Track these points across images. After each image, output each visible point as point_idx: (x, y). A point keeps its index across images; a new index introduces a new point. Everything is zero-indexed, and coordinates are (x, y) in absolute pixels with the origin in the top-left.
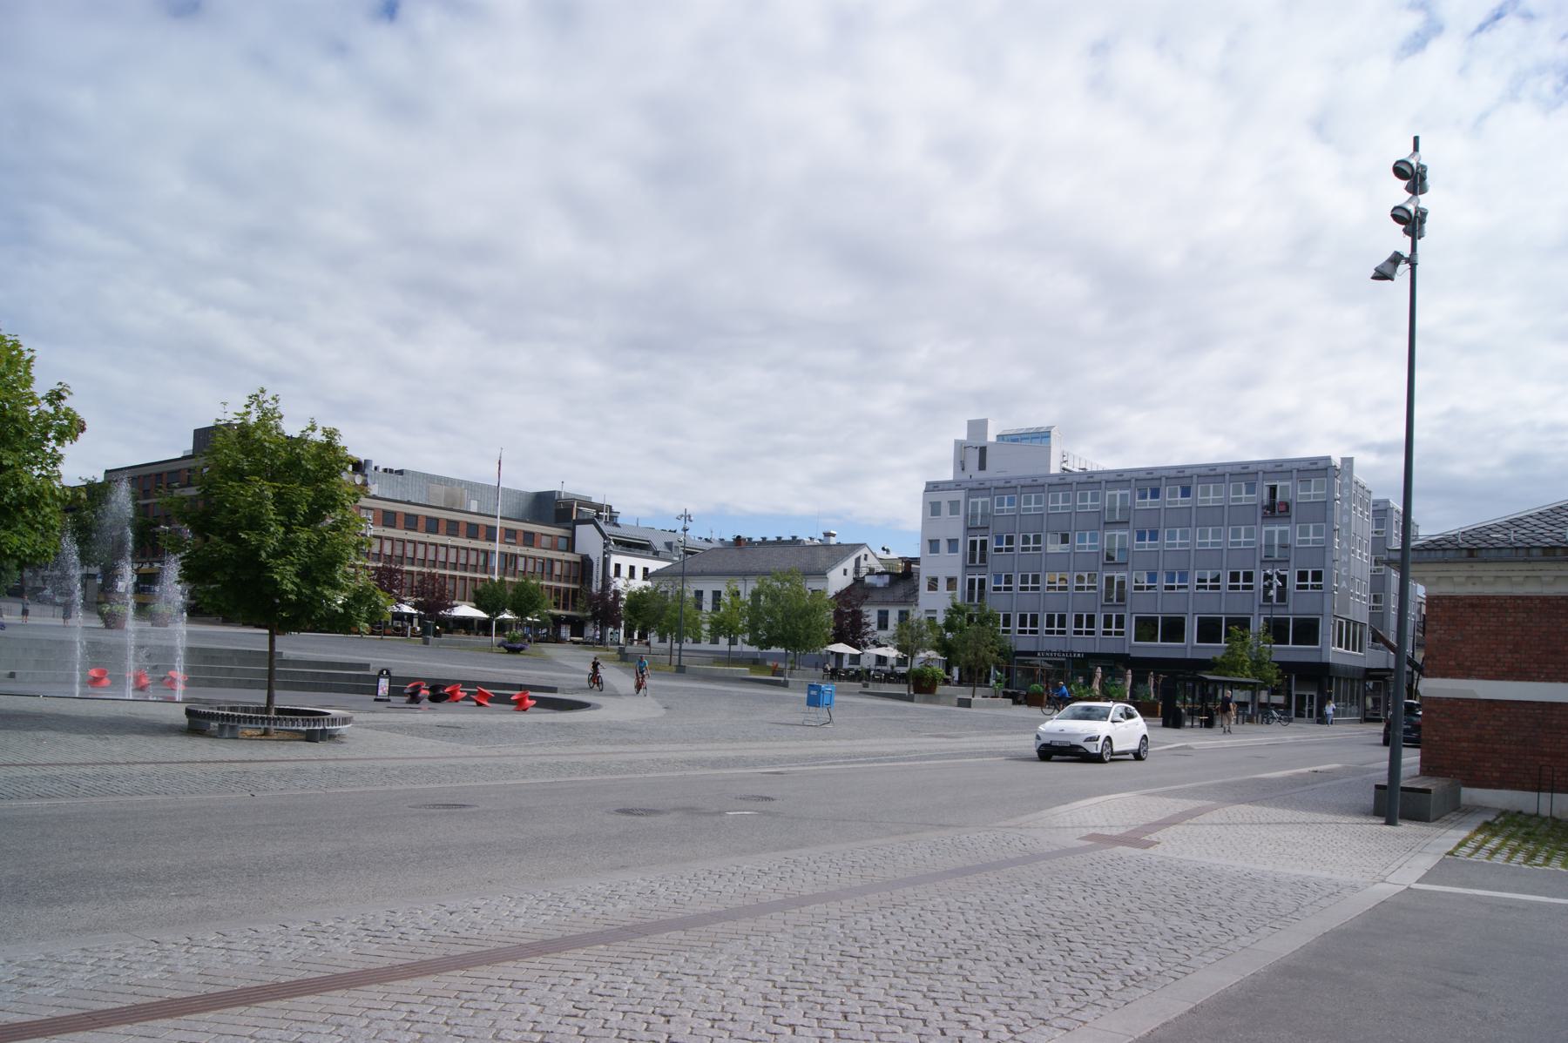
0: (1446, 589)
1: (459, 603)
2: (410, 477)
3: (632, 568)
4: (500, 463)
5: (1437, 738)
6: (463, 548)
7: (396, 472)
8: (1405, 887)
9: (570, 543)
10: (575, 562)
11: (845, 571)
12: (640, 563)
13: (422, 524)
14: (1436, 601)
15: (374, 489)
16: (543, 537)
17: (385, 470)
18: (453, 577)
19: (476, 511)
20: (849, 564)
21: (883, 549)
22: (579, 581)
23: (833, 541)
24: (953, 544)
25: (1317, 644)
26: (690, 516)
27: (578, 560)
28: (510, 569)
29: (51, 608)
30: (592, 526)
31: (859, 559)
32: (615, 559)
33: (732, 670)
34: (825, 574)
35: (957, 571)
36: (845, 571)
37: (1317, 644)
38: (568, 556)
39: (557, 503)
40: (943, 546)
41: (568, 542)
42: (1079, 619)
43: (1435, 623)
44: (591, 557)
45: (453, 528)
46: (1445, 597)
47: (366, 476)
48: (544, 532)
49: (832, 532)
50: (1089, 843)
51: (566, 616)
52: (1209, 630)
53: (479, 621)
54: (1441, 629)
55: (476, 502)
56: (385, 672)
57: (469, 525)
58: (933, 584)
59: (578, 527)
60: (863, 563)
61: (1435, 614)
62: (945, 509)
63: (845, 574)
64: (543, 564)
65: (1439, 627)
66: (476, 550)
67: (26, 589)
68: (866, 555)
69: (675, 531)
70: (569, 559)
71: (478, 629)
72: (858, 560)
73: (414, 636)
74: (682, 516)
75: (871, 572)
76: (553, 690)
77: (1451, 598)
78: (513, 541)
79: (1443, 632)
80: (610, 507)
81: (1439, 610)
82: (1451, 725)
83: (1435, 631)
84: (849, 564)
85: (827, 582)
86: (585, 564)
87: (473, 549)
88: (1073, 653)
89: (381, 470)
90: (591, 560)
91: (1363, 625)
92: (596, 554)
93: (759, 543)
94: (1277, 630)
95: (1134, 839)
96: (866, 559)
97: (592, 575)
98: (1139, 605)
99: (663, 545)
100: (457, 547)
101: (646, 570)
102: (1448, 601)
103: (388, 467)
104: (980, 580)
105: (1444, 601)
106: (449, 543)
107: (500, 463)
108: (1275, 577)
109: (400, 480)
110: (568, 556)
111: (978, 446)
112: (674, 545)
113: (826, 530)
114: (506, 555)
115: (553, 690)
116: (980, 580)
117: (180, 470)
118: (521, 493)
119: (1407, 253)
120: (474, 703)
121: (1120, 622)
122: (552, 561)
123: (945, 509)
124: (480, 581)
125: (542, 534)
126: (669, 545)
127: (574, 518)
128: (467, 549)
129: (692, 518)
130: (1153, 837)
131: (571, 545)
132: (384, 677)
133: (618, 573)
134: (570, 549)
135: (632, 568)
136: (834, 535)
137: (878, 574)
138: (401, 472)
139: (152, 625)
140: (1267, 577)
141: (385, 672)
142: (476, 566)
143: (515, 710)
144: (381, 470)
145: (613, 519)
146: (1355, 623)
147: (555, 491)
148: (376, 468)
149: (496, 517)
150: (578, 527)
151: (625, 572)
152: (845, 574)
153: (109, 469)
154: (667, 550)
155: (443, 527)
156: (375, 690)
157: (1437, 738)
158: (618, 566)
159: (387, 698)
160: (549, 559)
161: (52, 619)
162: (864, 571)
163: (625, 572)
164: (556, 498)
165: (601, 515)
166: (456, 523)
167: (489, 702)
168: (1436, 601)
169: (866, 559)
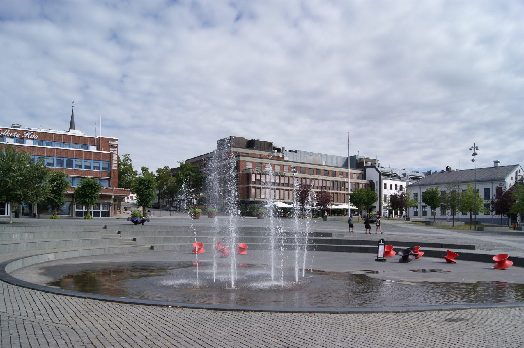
1: (343, 204)
2: (300, 153)
3: (391, 185)
4: (348, 139)
6: (324, 180)
7: (294, 151)
9: (364, 176)
10: (367, 184)
11: (512, 177)
12: (394, 183)
15: (286, 159)
16: (353, 174)
17: (290, 151)
18: (333, 193)
19: (325, 165)
20: (513, 174)
23: (499, 165)
25: (76, 216)
26: (477, 147)
27: (369, 183)
28: (343, 188)
29: (170, 212)
30: (373, 169)
32: (384, 182)
33: (502, 228)
34: (504, 179)
36: (512, 177)
37: (76, 216)
38: (364, 181)
39: (357, 160)
41: (363, 176)
44: (374, 181)
45: (319, 172)
47: (283, 153)
48: (353, 172)
49: (498, 161)
53: (332, 210)
55: (325, 162)
56: (382, 241)
59: (367, 170)
60: (518, 174)
63: (512, 179)
64: (355, 185)
66: (330, 181)
67: (161, 206)
68: (519, 170)
69: (405, 169)
70: (365, 183)
71: (331, 213)
72: (516, 173)
73: (314, 217)
74: (472, 147)
76: (473, 248)
78: (342, 176)
84: (513, 174)
85: (506, 183)
86: (371, 185)
87: (328, 180)
89: (288, 151)
90: (374, 183)
92: (376, 180)
93: (440, 173)
96: (519, 172)
97: (374, 189)
99: (402, 175)
100: (322, 180)
103: (291, 150)
106: (319, 178)
107: (348, 139)
109: (296, 155)
110: (364, 181)
112: (406, 175)
113: (496, 160)
114: (341, 182)
115: (473, 248)
118: (342, 157)
120: (445, 261)
122: (358, 184)
124: (331, 193)
125: (353, 173)
126: (404, 175)
127: (365, 166)
128: (326, 180)
129: (478, 148)
131: (364, 176)
132: (382, 245)
133: (385, 188)
134: (364, 178)
135: (391, 185)
136: (499, 162)
138: (296, 151)
139: (209, 217)
141: (382, 241)
142: (330, 187)
143: (495, 268)
144: (288, 151)
147: (355, 156)
148: (286, 151)
150: (367, 170)
151: (388, 186)
152: (512, 179)
153: (187, 159)
154: (404, 177)
156: (377, 251)
158: (385, 184)
159: (383, 258)
160: (357, 183)
161: (170, 216)
163: (388, 186)
164: (356, 158)
165: (373, 164)
166: (325, 175)
167: (456, 259)
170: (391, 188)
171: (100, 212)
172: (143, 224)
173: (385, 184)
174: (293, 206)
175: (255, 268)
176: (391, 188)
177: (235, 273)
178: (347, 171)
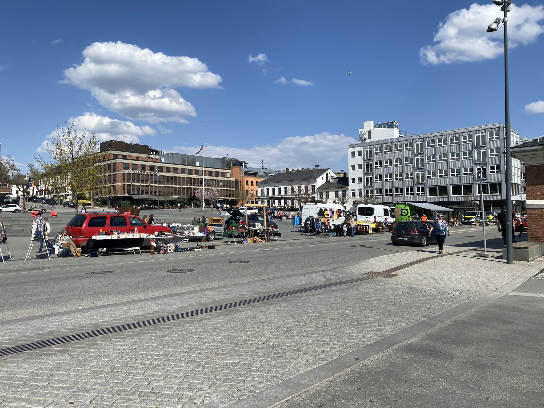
0: (533, 163)
3: (252, 182)
5: (534, 225)
8: (505, 294)
11: (323, 178)
13: (179, 171)
14: (530, 168)
21: (341, 170)
22: (235, 187)
23: (318, 168)
24: (360, 166)
31: (327, 173)
35: (362, 175)
36: (323, 178)
40: (357, 167)
42: (407, 189)
43: (530, 177)
46: (534, 166)
50: (393, 273)
51: (231, 199)
52: (457, 190)
54: (533, 179)
57: (216, 172)
58: (353, 180)
60: (329, 175)
61: (530, 173)
62: (357, 154)
65: (532, 179)
68: (330, 172)
72: (327, 174)
75: (332, 178)
77: (536, 166)
79: (533, 180)
80: (244, 162)
81: (531, 171)
82: (541, 219)
83: (530, 180)
84: (324, 175)
88: (406, 202)
91: (518, 185)
94: (484, 188)
95: (389, 273)
96: (330, 174)
98: (430, 182)
101: (257, 182)
102: (535, 167)
104: (370, 178)
105: (533, 167)
108: (482, 169)
111: (368, 130)
116: (370, 178)
117: (137, 164)
119: (502, 17)
121: (423, 189)
123: (357, 154)
130: (396, 273)
133: (247, 184)
135: (252, 182)
137: (334, 178)
140: (478, 169)
145: (245, 166)
146: (516, 184)
149: (204, 167)
151: (250, 183)
155: (187, 172)
157: (534, 225)
158: (247, 182)
162: (329, 178)
163: (250, 183)
166: (177, 169)
168: (530, 168)
169: (330, 174)
170: (252, 184)
171: (494, 170)
172: (41, 216)
173: (247, 182)
174: (522, 198)
175: (415, 287)
176: (252, 184)
177: (432, 326)
178: (201, 169)
